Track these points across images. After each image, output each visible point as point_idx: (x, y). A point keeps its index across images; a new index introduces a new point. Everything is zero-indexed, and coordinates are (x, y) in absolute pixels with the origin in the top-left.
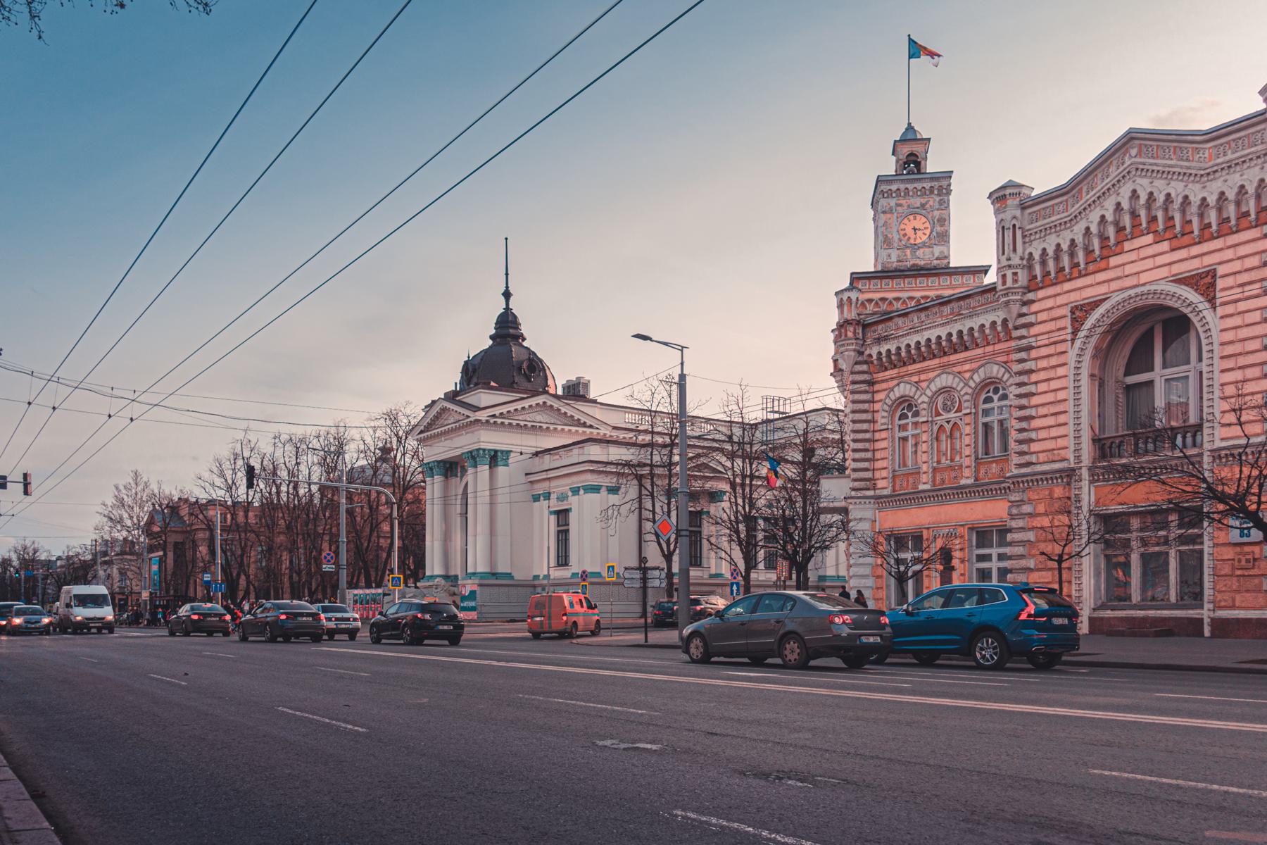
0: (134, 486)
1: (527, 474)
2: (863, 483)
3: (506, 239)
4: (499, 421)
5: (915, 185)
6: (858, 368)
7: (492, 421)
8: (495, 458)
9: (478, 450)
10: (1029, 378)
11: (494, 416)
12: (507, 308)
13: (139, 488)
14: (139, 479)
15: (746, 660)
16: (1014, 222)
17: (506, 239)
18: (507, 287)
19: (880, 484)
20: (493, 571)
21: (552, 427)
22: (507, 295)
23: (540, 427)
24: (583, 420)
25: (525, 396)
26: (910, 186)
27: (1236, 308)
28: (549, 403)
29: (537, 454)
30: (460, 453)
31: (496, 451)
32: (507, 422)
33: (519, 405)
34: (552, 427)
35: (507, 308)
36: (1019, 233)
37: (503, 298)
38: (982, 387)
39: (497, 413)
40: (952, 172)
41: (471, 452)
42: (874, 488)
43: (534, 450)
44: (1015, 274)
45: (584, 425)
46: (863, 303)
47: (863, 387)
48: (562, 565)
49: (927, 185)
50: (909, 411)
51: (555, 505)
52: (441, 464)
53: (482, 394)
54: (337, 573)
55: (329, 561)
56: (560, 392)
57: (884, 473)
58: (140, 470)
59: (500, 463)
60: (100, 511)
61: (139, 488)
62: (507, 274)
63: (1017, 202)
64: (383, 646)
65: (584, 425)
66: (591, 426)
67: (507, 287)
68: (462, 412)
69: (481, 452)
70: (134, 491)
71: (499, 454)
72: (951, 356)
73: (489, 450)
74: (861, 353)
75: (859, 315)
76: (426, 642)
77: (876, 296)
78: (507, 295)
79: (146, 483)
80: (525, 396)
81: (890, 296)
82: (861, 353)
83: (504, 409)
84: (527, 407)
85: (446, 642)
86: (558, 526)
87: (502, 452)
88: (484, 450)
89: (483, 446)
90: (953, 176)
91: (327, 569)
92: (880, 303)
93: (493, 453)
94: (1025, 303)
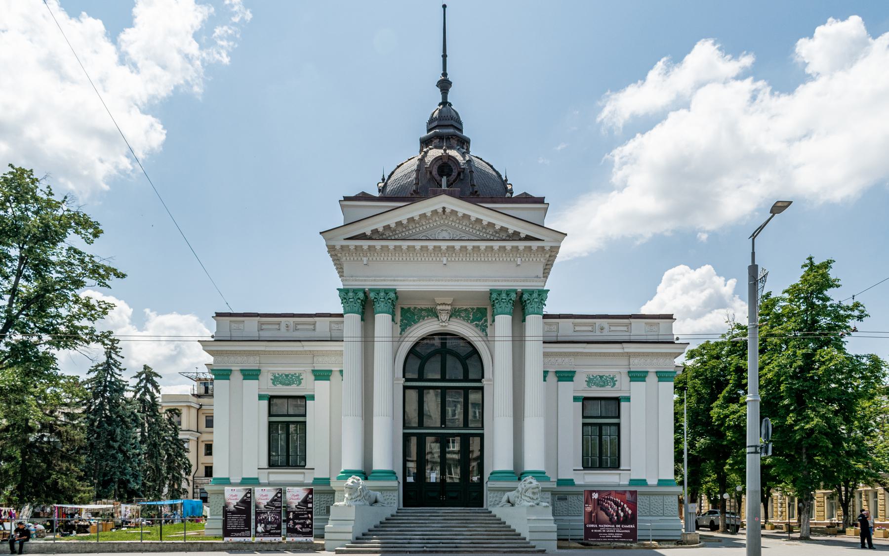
3: (444, 6)
17: (444, 6)
18: (445, 74)
35: (445, 103)
48: (593, 468)
67: (445, 74)
73: (508, 293)
78: (444, 85)
93: (513, 296)
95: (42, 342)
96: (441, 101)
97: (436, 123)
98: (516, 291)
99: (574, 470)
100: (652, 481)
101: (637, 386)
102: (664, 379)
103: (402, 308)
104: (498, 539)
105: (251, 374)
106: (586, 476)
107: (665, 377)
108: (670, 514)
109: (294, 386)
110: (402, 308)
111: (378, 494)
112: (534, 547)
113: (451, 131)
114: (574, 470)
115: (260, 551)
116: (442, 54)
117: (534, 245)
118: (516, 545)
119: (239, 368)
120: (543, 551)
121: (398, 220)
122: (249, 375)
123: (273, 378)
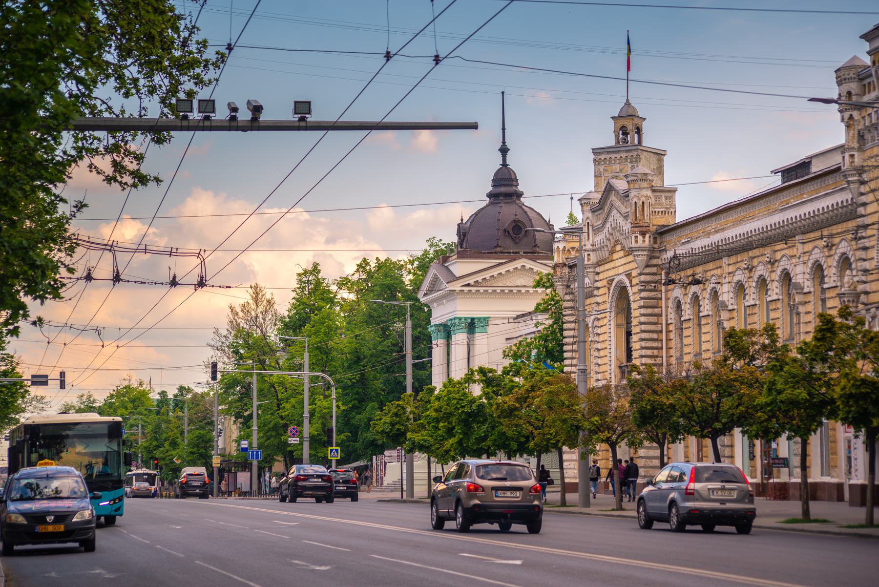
0: (253, 306)
1: (507, 339)
3: (503, 93)
4: (474, 289)
5: (616, 155)
6: (647, 270)
7: (466, 289)
10: (866, 255)
11: (468, 285)
12: (505, 165)
13: (260, 309)
14: (260, 296)
15: (699, 527)
16: (588, 221)
17: (503, 93)
18: (504, 142)
21: (523, 290)
22: (504, 151)
25: (504, 261)
26: (613, 156)
28: (528, 266)
29: (518, 317)
31: (473, 319)
32: (482, 289)
33: (495, 272)
34: (523, 290)
35: (505, 165)
36: (590, 228)
37: (500, 153)
39: (472, 282)
43: (514, 315)
44: (589, 255)
46: (569, 250)
49: (624, 155)
52: (441, 328)
53: (457, 264)
54: (301, 444)
55: (294, 434)
58: (261, 284)
60: (212, 343)
61: (260, 309)
62: (504, 129)
63: (588, 208)
64: (652, 531)
67: (504, 142)
70: (253, 314)
71: (476, 321)
73: (466, 319)
74: (568, 287)
75: (566, 259)
76: (717, 528)
78: (504, 151)
79: (269, 302)
80: (504, 261)
82: (568, 287)
83: (479, 278)
84: (519, 268)
85: (733, 529)
87: (479, 319)
88: (460, 319)
89: (459, 315)
91: (292, 442)
93: (469, 321)
94: (863, 183)
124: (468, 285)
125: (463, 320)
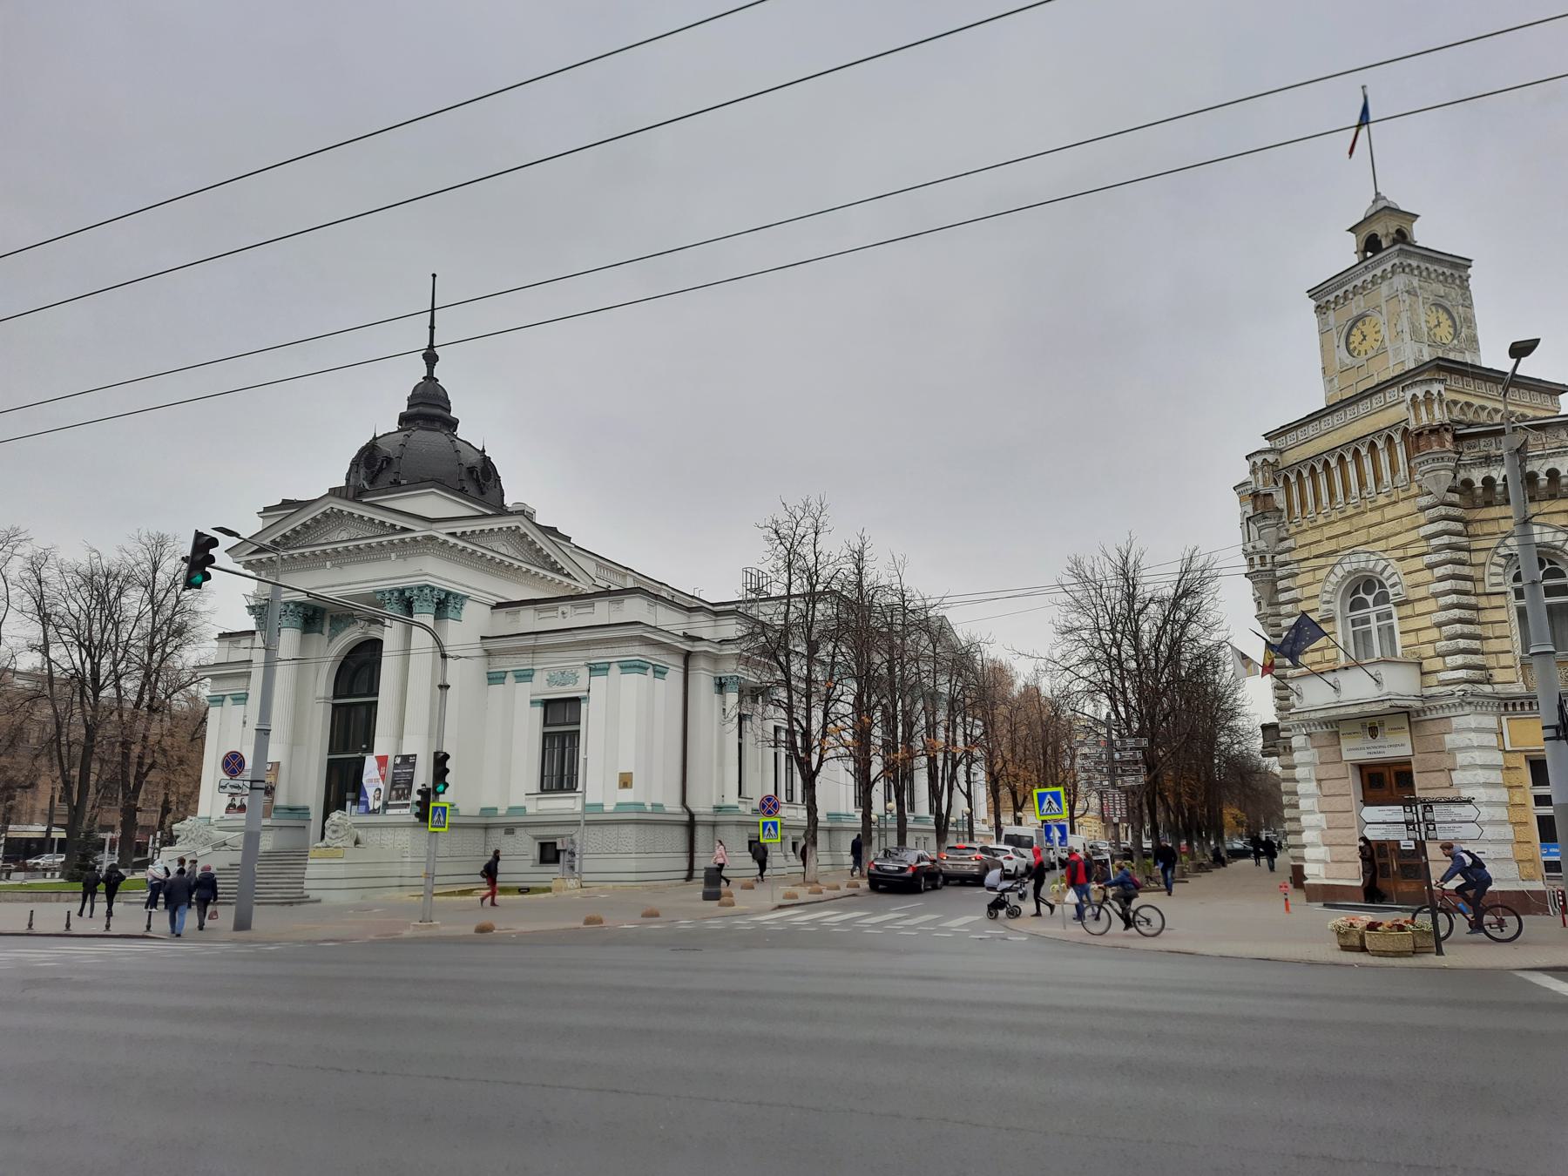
2: (1471, 672)
3: (434, 276)
7: (452, 540)
8: (444, 604)
9: (421, 589)
12: (430, 377)
17: (434, 276)
19: (1499, 675)
20: (291, 805)
22: (431, 358)
23: (511, 564)
24: (561, 564)
27: (1419, 534)
28: (523, 530)
30: (370, 590)
31: (448, 594)
32: (470, 547)
35: (430, 377)
38: (637, 663)
40: (1418, 216)
41: (402, 592)
42: (1489, 681)
45: (560, 571)
47: (1459, 526)
48: (550, 790)
50: (1368, 591)
51: (542, 687)
52: (301, 609)
56: (1529, 469)
57: (1506, 660)
59: (451, 614)
65: (560, 571)
66: (568, 575)
68: (496, 527)
69: (427, 591)
72: (1545, 504)
73: (391, 592)
77: (1462, 399)
78: (431, 358)
80: (490, 513)
81: (1477, 402)
86: (545, 724)
87: (456, 596)
90: (1419, 219)
92: (1493, 413)
95: (47, 692)
96: (426, 375)
97: (419, 401)
98: (397, 590)
99: (527, 794)
100: (609, 807)
101: (598, 682)
102: (495, 681)
103: (332, 616)
104: (267, 883)
105: (525, 676)
106: (540, 802)
107: (497, 678)
108: (607, 852)
109: (569, 687)
110: (332, 616)
111: (360, 833)
112: (308, 897)
113: (438, 411)
114: (527, 794)
115: (37, 901)
116: (429, 324)
117: (407, 536)
118: (294, 896)
119: (583, 663)
120: (319, 901)
121: (372, 516)
122: (520, 676)
123: (548, 677)
124: (453, 534)
125: (427, 591)
